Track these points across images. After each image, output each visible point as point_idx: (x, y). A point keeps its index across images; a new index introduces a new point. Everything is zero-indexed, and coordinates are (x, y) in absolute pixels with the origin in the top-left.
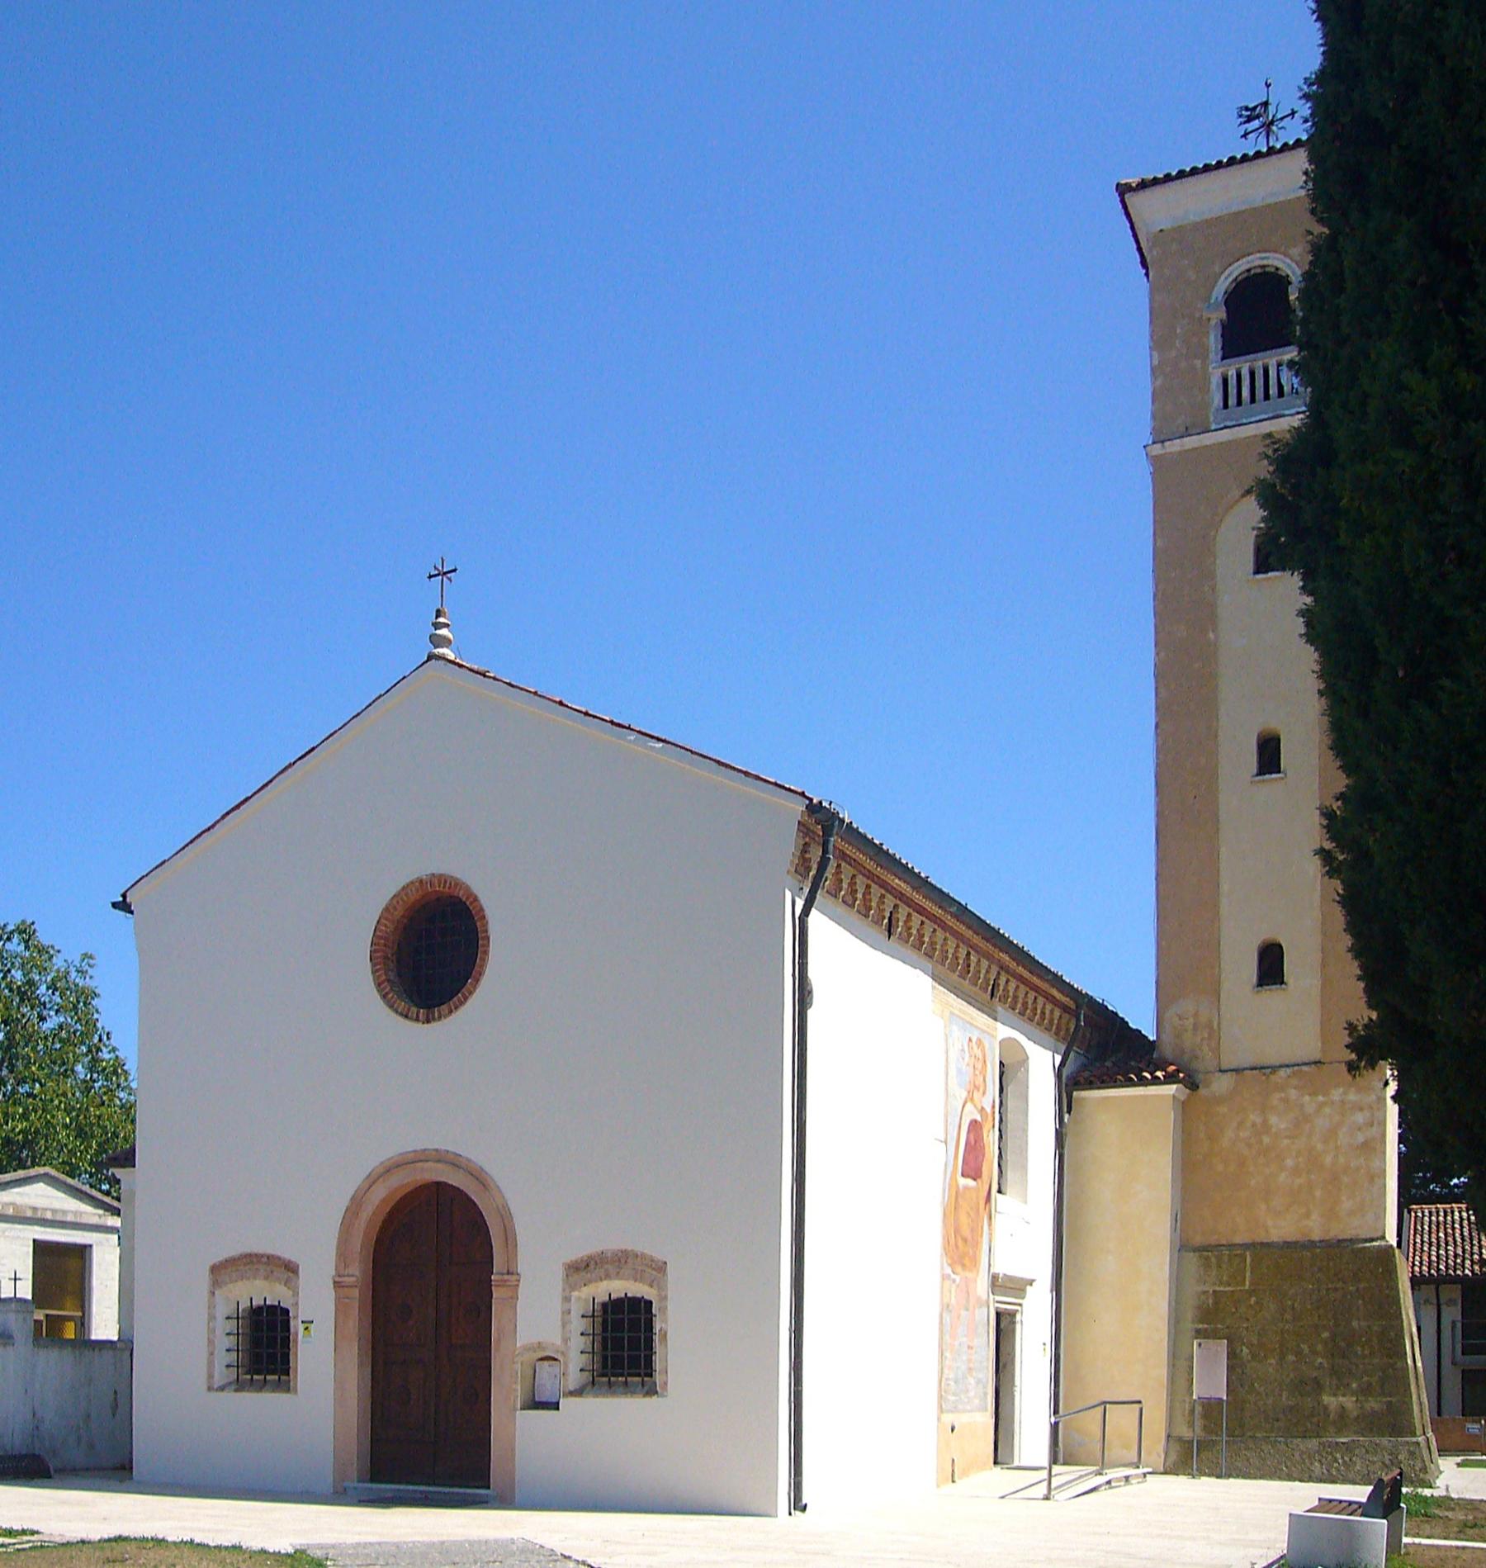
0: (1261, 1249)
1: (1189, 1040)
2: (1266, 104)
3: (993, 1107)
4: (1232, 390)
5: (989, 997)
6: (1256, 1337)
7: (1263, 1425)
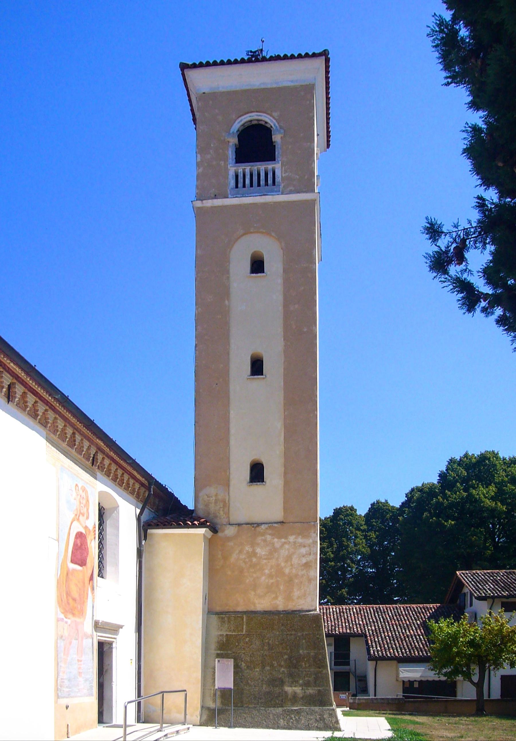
0: (251, 614)
1: (212, 508)
2: (262, 50)
3: (95, 527)
4: (241, 180)
5: (91, 465)
6: (249, 658)
7: (253, 701)
